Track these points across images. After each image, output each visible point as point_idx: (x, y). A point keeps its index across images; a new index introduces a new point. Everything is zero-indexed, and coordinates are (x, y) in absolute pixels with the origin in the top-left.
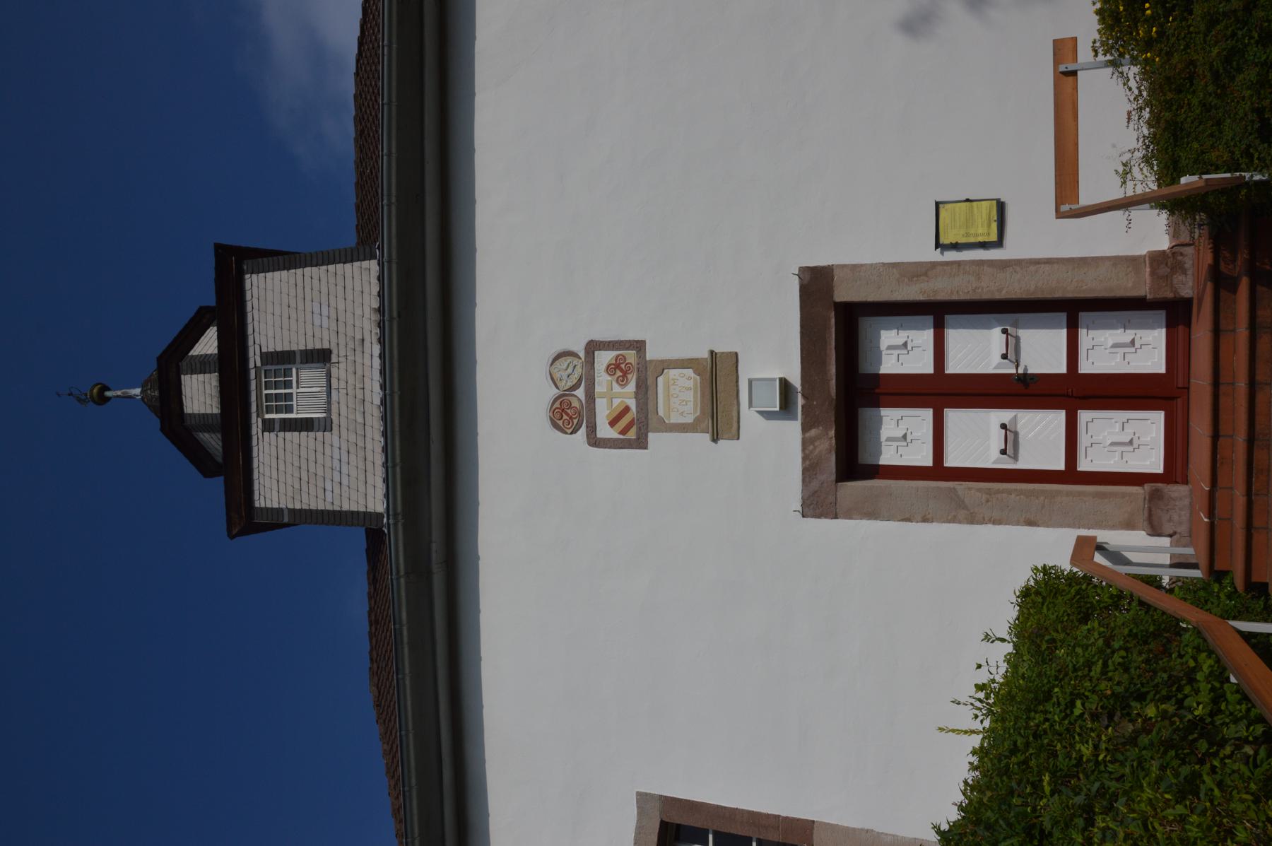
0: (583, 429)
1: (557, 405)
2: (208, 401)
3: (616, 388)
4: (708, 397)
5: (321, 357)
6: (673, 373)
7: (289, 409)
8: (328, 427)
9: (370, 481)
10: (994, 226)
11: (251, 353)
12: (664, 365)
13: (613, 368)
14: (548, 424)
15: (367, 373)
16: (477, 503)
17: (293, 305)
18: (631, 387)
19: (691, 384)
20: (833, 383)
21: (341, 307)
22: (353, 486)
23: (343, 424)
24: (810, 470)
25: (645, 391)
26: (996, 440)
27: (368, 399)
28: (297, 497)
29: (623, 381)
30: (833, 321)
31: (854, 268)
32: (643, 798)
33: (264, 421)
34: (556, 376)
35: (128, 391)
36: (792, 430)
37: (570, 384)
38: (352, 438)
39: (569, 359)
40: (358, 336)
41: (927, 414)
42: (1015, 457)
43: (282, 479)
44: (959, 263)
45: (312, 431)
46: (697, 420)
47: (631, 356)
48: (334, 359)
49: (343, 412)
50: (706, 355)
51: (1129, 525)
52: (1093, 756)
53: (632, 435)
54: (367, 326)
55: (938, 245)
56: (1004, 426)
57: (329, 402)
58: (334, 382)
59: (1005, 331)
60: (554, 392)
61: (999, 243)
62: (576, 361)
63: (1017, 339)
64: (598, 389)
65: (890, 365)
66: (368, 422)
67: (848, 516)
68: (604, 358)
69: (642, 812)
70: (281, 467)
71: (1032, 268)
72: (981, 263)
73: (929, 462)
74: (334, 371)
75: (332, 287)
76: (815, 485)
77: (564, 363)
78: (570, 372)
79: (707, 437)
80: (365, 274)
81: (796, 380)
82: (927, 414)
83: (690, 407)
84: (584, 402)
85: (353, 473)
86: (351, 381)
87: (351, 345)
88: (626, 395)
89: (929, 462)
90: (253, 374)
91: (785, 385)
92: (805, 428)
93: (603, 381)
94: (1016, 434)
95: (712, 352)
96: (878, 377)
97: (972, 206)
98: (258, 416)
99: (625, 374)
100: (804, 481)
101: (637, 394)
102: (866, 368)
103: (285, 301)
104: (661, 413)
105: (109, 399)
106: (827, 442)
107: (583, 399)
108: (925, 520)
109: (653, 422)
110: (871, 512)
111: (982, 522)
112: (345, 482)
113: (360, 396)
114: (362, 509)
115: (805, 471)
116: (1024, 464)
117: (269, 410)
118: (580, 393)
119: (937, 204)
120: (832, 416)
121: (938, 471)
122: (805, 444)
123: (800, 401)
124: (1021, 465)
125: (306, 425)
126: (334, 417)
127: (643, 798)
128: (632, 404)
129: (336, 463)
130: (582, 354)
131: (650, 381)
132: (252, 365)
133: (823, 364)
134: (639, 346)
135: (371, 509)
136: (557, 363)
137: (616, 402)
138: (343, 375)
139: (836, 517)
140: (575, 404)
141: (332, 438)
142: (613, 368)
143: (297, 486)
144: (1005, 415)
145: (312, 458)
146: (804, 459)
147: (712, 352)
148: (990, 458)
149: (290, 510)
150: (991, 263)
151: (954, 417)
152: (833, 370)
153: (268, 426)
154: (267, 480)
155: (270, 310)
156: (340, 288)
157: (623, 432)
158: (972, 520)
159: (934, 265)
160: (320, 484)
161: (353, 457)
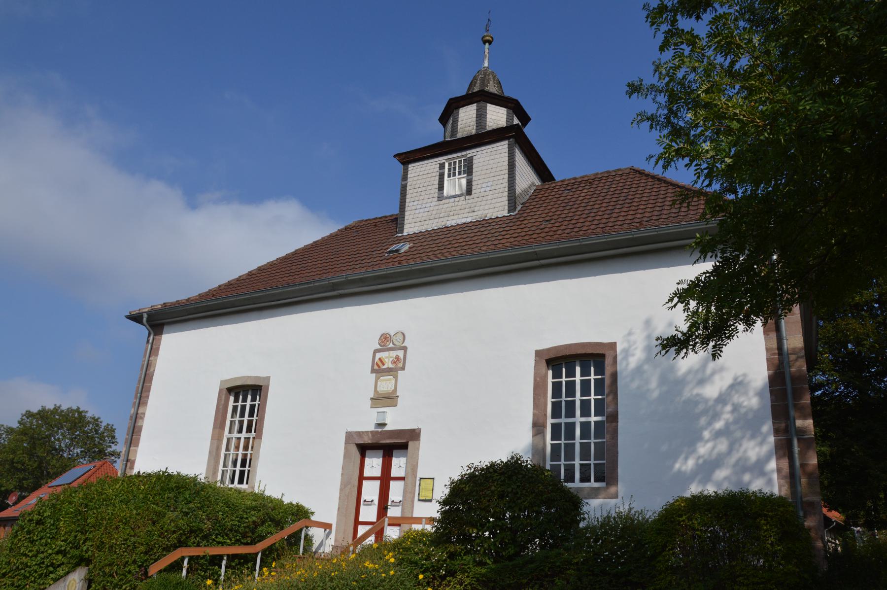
0: (380, 347)
1: (388, 336)
2: (464, 122)
3: (391, 359)
4: (386, 396)
5: (469, 191)
6: (393, 382)
7: (449, 176)
8: (440, 199)
9: (417, 224)
10: (424, 498)
11: (473, 151)
12: (396, 378)
13: (398, 358)
14: (382, 333)
15: (460, 216)
16: (360, 305)
17: (493, 170)
18: (391, 366)
19: (389, 389)
20: (384, 442)
21: (489, 197)
22: (416, 216)
23: (441, 207)
24: (359, 434)
25: (389, 371)
26: (369, 499)
27: (450, 218)
28: (412, 187)
29: (394, 362)
30: (403, 441)
31: (418, 449)
32: (268, 378)
33: (444, 163)
34: (397, 335)
35: (487, 58)
36: (372, 428)
37: (394, 340)
38: (434, 212)
39: (402, 340)
40: (476, 209)
41: (379, 475)
42: (364, 505)
43: (420, 178)
44: (415, 486)
45: (439, 191)
46: (378, 392)
47: (401, 365)
48: (468, 197)
49: (446, 205)
50: (398, 394)
51: (336, 540)
52: (386, 545)
53: (376, 367)
54: (480, 213)
55: (421, 478)
56: (373, 501)
57: (140, 399)
58: (457, 199)
59: (400, 502)
60: (392, 335)
61: (419, 500)
62: (401, 343)
63: (399, 506)
64: (391, 352)
65: (395, 461)
66: (441, 220)
67: (345, 448)
68: (401, 353)
69: (265, 378)
70: (425, 176)
71: (411, 511)
72: (414, 494)
73: (365, 475)
74: (462, 198)
75: (497, 191)
76: (355, 436)
77: (401, 338)
78: (398, 340)
79: (372, 396)
80: (501, 209)
81: (387, 428)
82: (379, 475)
83: (382, 389)
84: (258, 394)
85: (420, 215)
86: (458, 208)
87: (473, 205)
88: (388, 364)
89: (365, 475)
90: (464, 153)
91: (384, 425)
92: (372, 432)
93: (393, 354)
94: (371, 505)
95: (398, 397)
96: (391, 457)
97: (429, 490)
98: (446, 159)
99: (395, 363)
100: (356, 432)
101: (388, 368)
102: (395, 452)
103: (495, 166)
104: (381, 378)
105: (485, 44)
106: (367, 440)
107: (389, 346)
108: (342, 474)
109: (379, 375)
110: (346, 455)
111: (340, 494)
112: (417, 211)
113: (452, 213)
114: (405, 222)
115: (359, 432)
116: (362, 507)
117: (450, 164)
118: (391, 345)
119: (433, 478)
120: (375, 442)
121: (362, 478)
122: (367, 432)
123: (380, 430)
124: (362, 506)
125: (441, 187)
126: (443, 201)
127: (268, 378)
128: (385, 367)
129: (424, 206)
130: (403, 345)
131: (391, 373)
132: (468, 152)
133: (389, 438)
134: (403, 368)
135: (406, 226)
136: (402, 335)
137: (386, 360)
138: (460, 203)
139: (345, 444)
140: (388, 343)
141: (435, 202)
142: (398, 358)
143: (417, 186)
144: (376, 502)
145: (428, 192)
146: (363, 432)
147: (398, 397)
148: (364, 496)
149: (406, 184)
150: (414, 497)
151: (377, 483)
152: (388, 441)
153: (442, 166)
154: (419, 170)
155: (492, 157)
156: (496, 196)
157: (377, 364)
158: (341, 490)
159: (416, 477)
160: (417, 199)
161: (426, 214)
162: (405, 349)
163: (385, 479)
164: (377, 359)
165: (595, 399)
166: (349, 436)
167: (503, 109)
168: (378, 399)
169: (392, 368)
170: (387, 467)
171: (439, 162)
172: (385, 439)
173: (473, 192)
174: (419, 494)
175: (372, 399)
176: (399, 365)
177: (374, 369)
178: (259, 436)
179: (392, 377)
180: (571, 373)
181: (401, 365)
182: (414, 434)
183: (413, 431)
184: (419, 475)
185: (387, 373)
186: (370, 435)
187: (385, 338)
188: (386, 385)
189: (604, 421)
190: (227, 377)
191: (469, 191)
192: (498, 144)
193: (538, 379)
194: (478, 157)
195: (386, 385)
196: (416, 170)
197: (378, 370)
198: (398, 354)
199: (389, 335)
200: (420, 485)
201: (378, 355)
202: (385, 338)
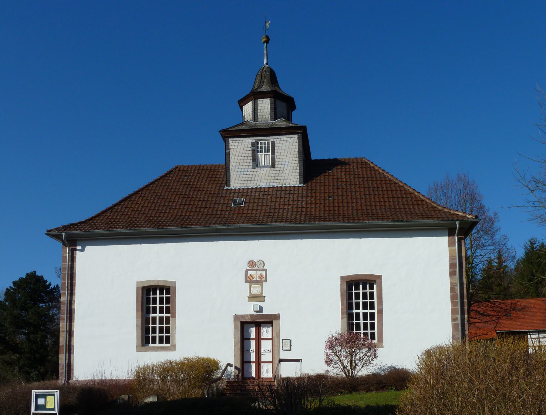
3: (258, 276)
8: (253, 167)
12: (262, 286)
13: (261, 275)
18: (258, 279)
24: (242, 316)
25: (257, 282)
29: (259, 277)
32: (175, 282)
47: (264, 279)
48: (272, 169)
49: (258, 171)
53: (248, 279)
68: (263, 273)
69: (172, 282)
88: (256, 278)
93: (259, 272)
99: (260, 278)
108: (234, 338)
111: (234, 348)
118: (256, 268)
122: (247, 315)
127: (175, 282)
128: (254, 279)
134: (266, 281)
135: (232, 183)
137: (255, 276)
146: (244, 315)
157: (249, 277)
162: (266, 270)
163: (258, 339)
164: (248, 275)
165: (370, 302)
166: (236, 317)
167: (285, 103)
168: (252, 297)
169: (259, 281)
170: (258, 333)
171: (251, 141)
172: (258, 319)
173: (276, 166)
174: (282, 347)
175: (248, 297)
176: (262, 280)
177: (247, 281)
178: (174, 316)
179: (259, 285)
180: (357, 288)
181: (264, 279)
182: (277, 317)
183: (275, 315)
184: (281, 338)
185: (256, 283)
186: (249, 317)
187: (252, 264)
188: (256, 289)
189: (170, 317)
190: (142, 280)
191: (273, 166)
192: (291, 136)
193: (343, 291)
194: (278, 142)
195: (256, 289)
196: (235, 144)
197: (250, 281)
198: (262, 273)
199: (254, 261)
200: (282, 342)
201: (249, 273)
202: (252, 264)
